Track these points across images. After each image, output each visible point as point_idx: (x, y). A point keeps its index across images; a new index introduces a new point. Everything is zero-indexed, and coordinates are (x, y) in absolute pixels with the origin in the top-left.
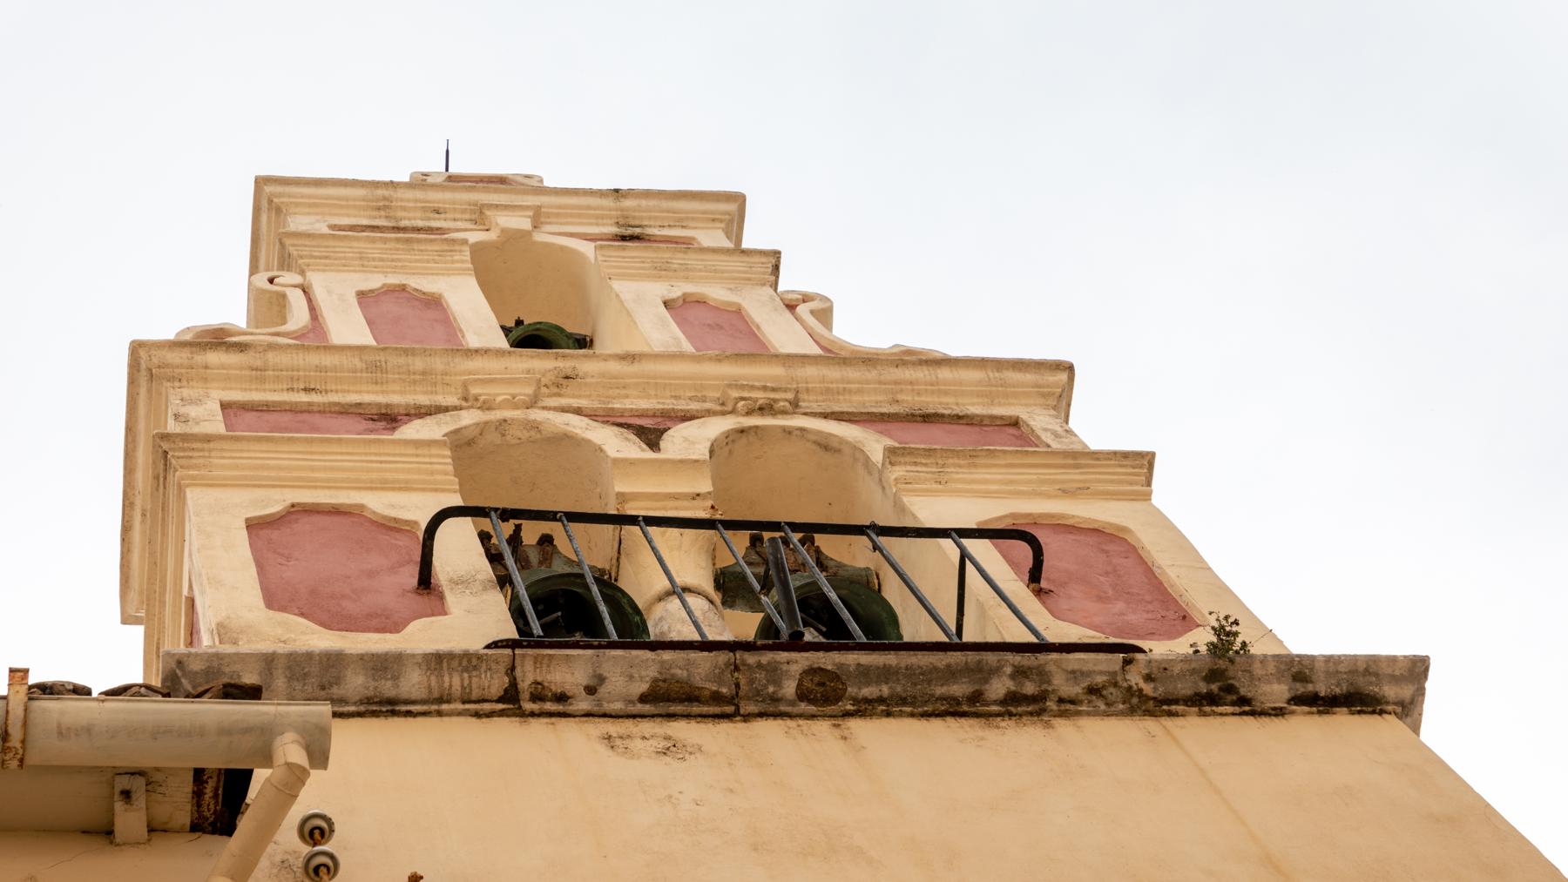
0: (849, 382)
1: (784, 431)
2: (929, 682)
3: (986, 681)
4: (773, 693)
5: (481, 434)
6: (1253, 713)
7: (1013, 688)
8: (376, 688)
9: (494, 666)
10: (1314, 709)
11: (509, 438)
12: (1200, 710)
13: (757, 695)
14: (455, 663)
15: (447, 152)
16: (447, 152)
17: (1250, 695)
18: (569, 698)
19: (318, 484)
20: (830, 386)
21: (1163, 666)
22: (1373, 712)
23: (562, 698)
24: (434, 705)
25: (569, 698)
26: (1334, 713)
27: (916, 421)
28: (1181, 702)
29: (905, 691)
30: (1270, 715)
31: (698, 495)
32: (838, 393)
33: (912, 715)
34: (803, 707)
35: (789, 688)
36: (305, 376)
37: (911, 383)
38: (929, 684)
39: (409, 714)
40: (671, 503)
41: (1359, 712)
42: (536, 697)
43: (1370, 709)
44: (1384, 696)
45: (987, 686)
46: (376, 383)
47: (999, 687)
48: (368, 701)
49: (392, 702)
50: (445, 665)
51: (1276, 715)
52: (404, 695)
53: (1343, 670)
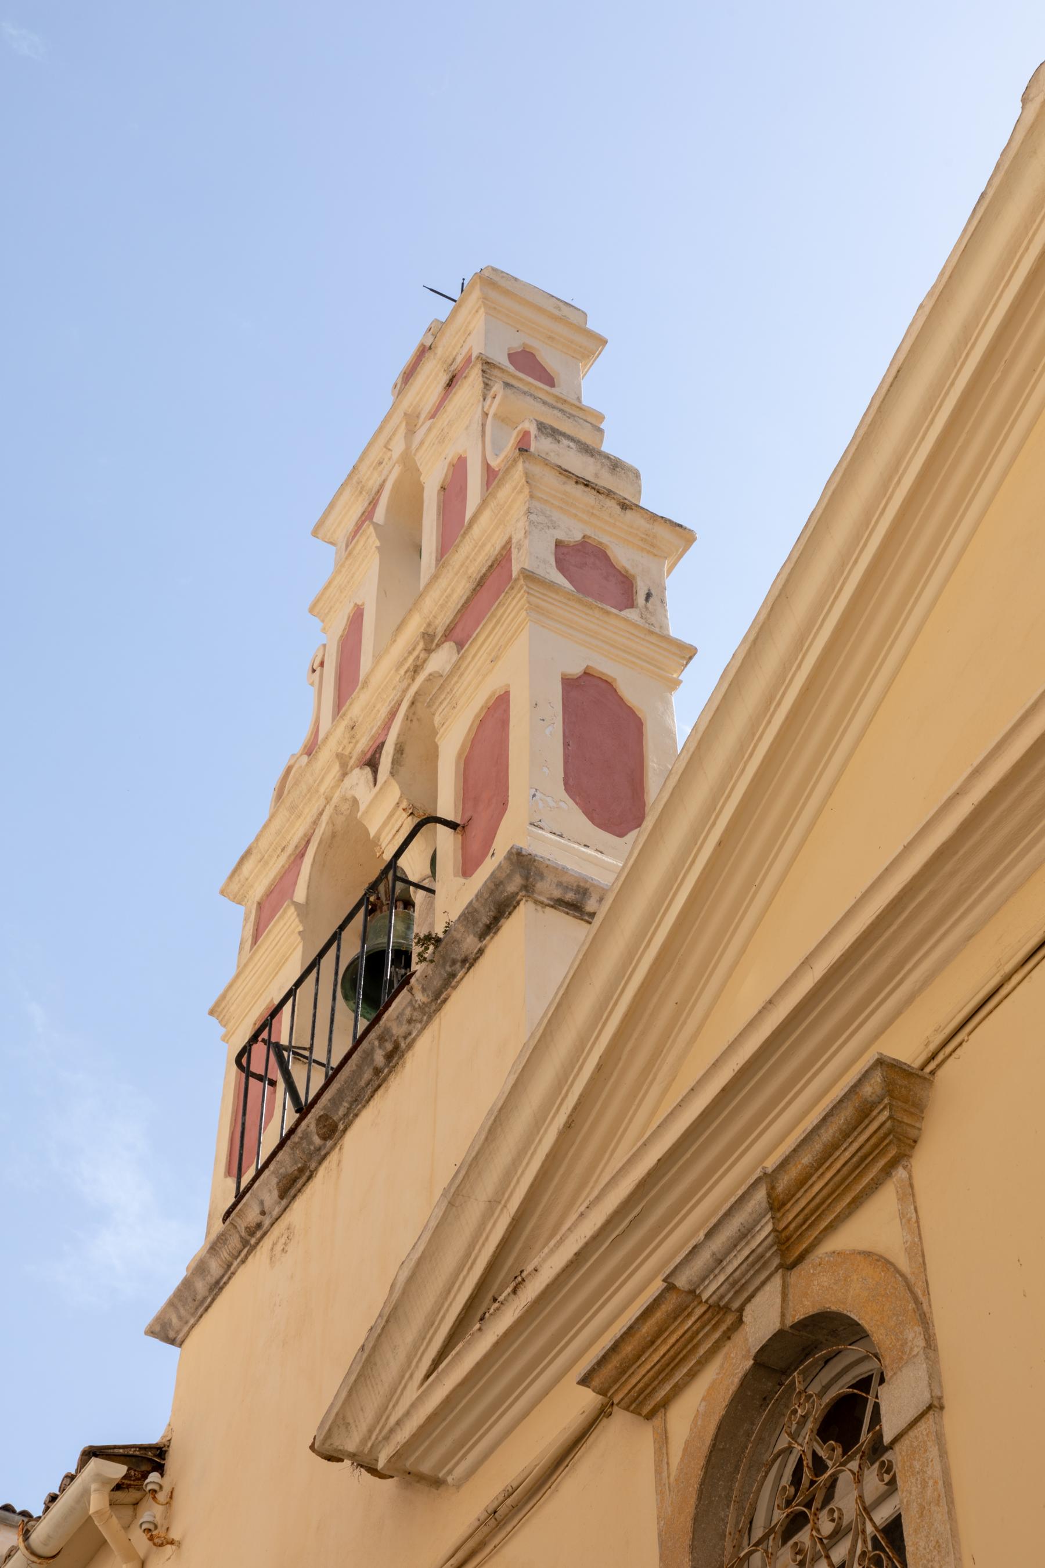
0: (445, 591)
1: (427, 680)
2: (356, 1084)
3: (373, 1060)
4: (315, 1148)
5: (334, 825)
6: (476, 959)
7: (384, 1053)
8: (207, 1283)
9: (230, 1233)
10: (491, 934)
11: (345, 813)
12: (452, 987)
13: (310, 1156)
14: (219, 1245)
15: (431, 290)
16: (431, 290)
17: (463, 956)
18: (261, 1223)
19: (261, 992)
20: (441, 602)
21: (424, 976)
22: (515, 907)
23: (259, 1226)
24: (228, 1271)
25: (261, 1223)
26: (501, 926)
27: (478, 591)
28: (443, 990)
29: (352, 1097)
30: (479, 957)
31: (398, 803)
32: (446, 602)
33: (364, 1106)
34: (329, 1143)
35: (317, 1140)
36: (276, 844)
37: (467, 558)
38: (357, 1085)
39: (226, 1283)
40: (393, 820)
41: (510, 914)
42: (252, 1234)
43: (512, 908)
44: (512, 893)
45: (375, 1063)
46: (299, 817)
47: (379, 1058)
48: (211, 1290)
49: (217, 1282)
50: (217, 1249)
51: (481, 954)
52: (218, 1277)
53: (487, 896)
